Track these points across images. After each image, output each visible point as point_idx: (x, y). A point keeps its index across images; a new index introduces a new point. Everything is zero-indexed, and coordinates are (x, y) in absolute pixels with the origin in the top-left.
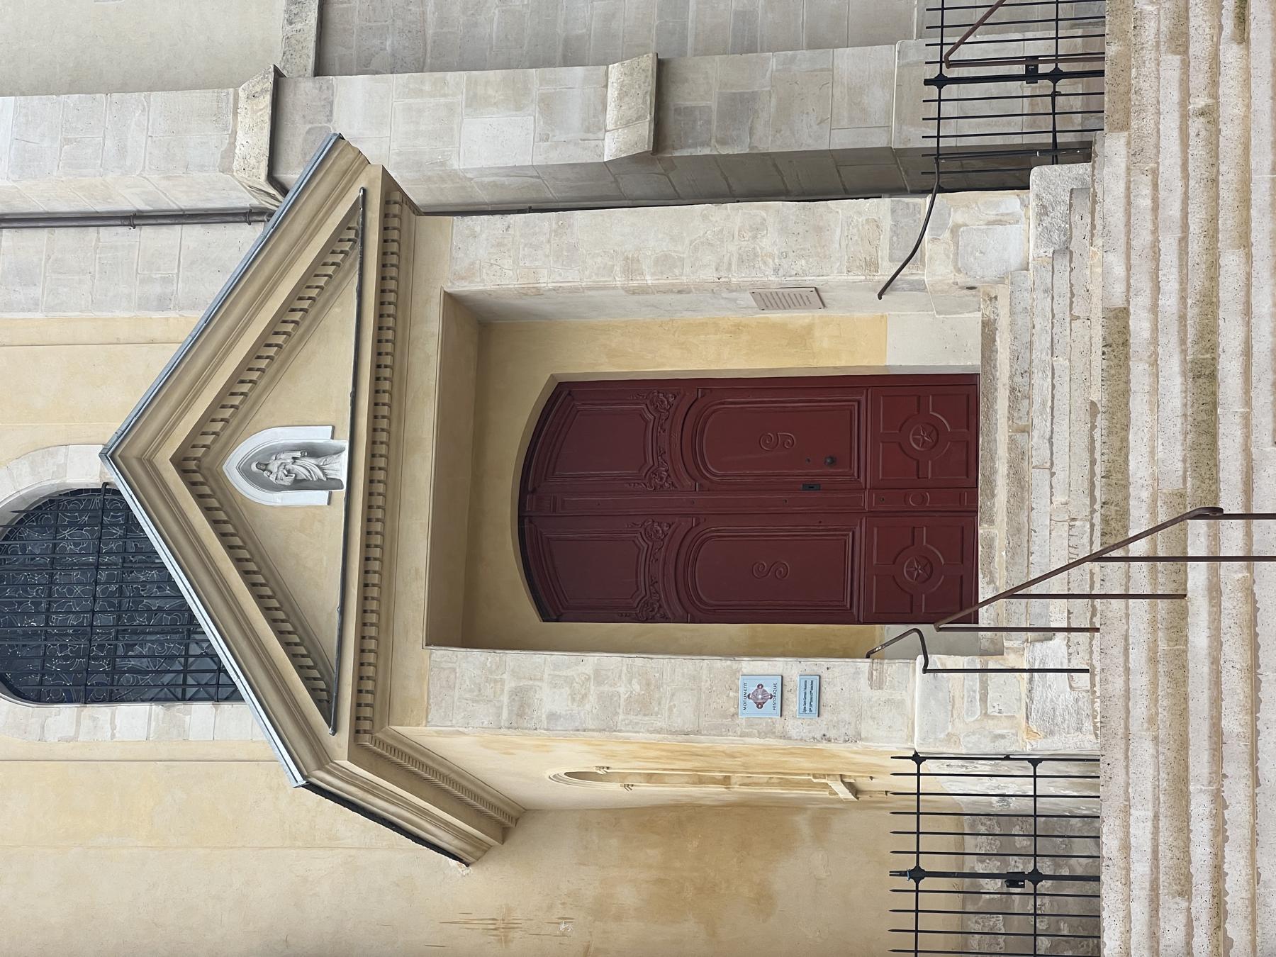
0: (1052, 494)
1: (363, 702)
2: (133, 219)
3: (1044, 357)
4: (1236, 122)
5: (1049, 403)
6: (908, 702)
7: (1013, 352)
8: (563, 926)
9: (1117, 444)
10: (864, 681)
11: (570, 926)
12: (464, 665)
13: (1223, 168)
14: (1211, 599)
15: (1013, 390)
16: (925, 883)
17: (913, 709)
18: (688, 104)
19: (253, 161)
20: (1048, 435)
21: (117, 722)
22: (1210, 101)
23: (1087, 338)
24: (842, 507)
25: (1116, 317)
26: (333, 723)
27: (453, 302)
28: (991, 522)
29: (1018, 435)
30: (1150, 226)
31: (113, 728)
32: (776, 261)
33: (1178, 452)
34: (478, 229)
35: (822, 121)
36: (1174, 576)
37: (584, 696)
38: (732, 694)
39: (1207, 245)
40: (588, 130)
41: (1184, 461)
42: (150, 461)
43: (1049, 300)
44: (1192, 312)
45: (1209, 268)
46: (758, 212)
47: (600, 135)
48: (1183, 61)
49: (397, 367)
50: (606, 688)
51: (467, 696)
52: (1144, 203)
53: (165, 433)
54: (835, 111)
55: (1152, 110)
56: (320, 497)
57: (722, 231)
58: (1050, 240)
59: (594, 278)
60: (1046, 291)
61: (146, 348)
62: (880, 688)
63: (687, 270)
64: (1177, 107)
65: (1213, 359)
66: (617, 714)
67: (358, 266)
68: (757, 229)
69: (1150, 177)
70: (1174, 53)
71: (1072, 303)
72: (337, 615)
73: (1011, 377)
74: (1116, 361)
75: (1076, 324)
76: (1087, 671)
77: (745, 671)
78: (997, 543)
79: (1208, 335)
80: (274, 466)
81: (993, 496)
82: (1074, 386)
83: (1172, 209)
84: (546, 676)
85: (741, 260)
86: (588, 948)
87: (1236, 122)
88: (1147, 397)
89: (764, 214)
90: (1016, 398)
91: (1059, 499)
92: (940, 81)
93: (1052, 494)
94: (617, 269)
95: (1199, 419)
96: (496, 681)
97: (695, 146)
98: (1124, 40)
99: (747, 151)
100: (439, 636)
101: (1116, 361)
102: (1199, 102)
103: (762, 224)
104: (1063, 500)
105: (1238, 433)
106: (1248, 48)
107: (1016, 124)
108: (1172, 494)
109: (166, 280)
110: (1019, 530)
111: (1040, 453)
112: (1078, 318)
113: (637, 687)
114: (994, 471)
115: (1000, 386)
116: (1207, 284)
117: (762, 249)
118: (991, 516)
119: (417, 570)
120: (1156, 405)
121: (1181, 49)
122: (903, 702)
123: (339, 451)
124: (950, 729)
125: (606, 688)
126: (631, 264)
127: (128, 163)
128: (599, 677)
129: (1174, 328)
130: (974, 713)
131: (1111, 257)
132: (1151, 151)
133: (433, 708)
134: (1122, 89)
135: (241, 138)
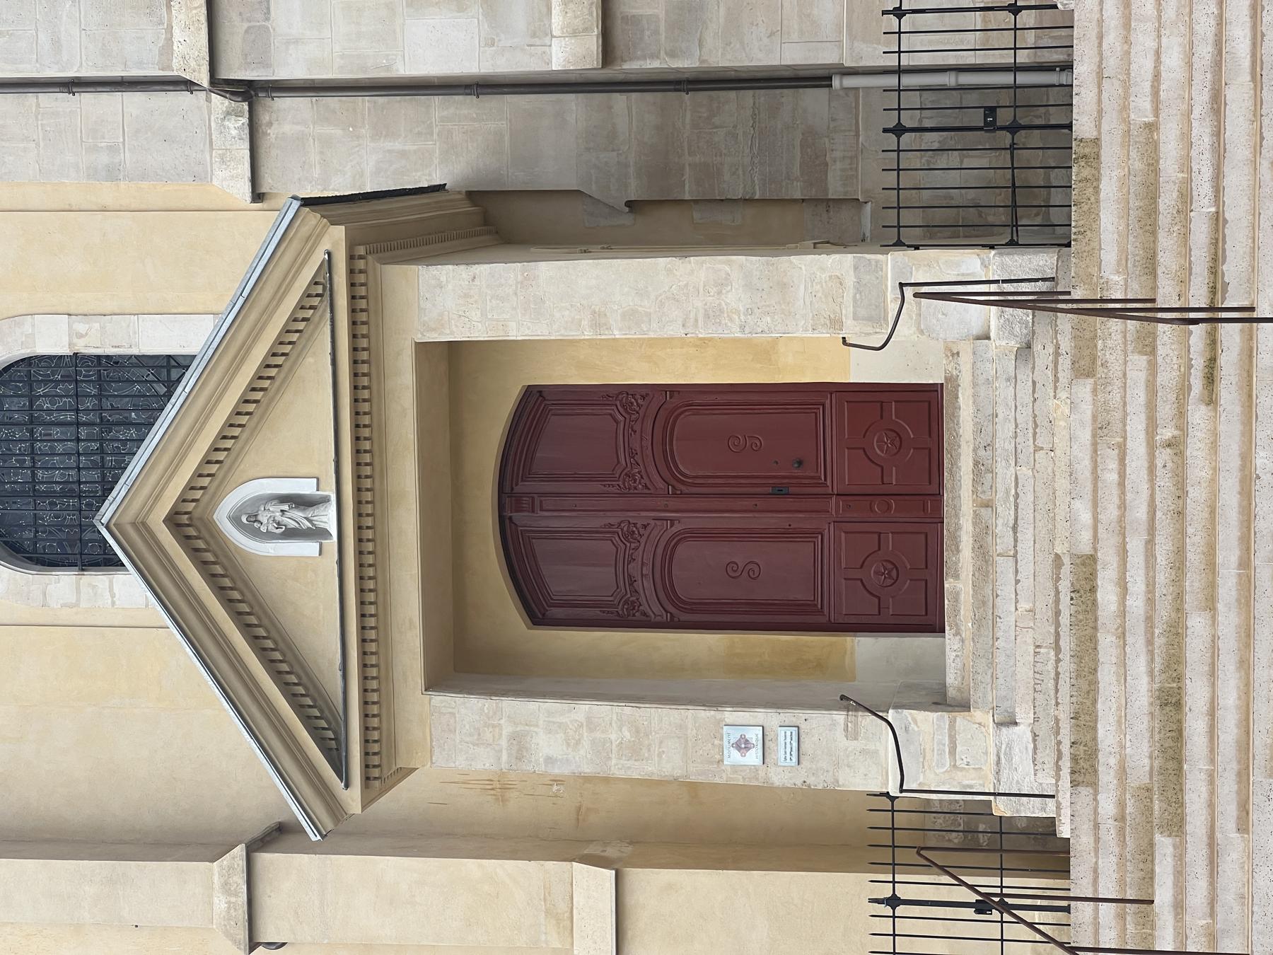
0: (1017, 602)
1: (371, 751)
2: (72, 85)
3: (1007, 446)
4: (1204, 485)
5: (1013, 492)
6: (882, 753)
7: (976, 424)
8: (555, 788)
9: (1085, 687)
10: (839, 733)
11: (562, 788)
12: (463, 711)
13: (1190, 530)
14: (1177, 914)
15: (976, 463)
16: (900, 910)
17: (886, 759)
18: (634, 12)
19: (193, 64)
20: (1011, 522)
21: (116, 590)
22: (1177, 433)
23: (1050, 470)
24: (809, 522)
25: (1083, 564)
26: (340, 766)
27: (423, 349)
28: (957, 577)
29: (983, 510)
30: (1116, 500)
31: (113, 596)
32: (742, 317)
33: (1145, 748)
34: (443, 279)
35: (772, 34)
36: (1141, 866)
37: (578, 742)
38: (716, 742)
39: (1173, 577)
40: (534, 35)
41: (1151, 757)
42: (144, 524)
43: (1011, 389)
44: (1159, 642)
45: (1175, 599)
46: (719, 266)
47: (547, 40)
48: (1149, 362)
49: (375, 426)
50: (598, 735)
51: (468, 739)
52: (1111, 477)
53: (156, 497)
54: (785, 22)
55: (1118, 383)
56: (308, 548)
57: (686, 285)
58: (1011, 333)
59: (563, 332)
60: (1008, 380)
61: (99, 215)
62: (856, 739)
63: (654, 325)
64: (1143, 409)
65: (1179, 688)
66: (610, 758)
67: (328, 315)
68: (722, 284)
69: (1116, 451)
70: (1141, 353)
71: (1035, 434)
72: (339, 674)
73: (975, 450)
74: (1084, 607)
75: (1040, 454)
76: (1053, 796)
77: (728, 721)
78: (962, 597)
79: (1177, 632)
80: (263, 518)
81: (958, 551)
82: (1038, 517)
83: (1140, 512)
84: (541, 722)
85: (707, 316)
86: (580, 808)
87: (1204, 485)
88: (1114, 669)
89: (727, 269)
90: (980, 472)
91: (1024, 605)
92: (899, 130)
93: (1017, 602)
94: (585, 323)
95: (1166, 745)
96: (494, 726)
97: (644, 58)
98: (1090, 284)
99: (697, 65)
100: (436, 681)
101: (1084, 607)
102: (1166, 433)
103: (726, 279)
104: (1028, 607)
105: (1204, 790)
106: (1215, 410)
107: (970, 40)
108: (1139, 788)
109: (112, 149)
110: (984, 603)
111: (1004, 540)
112: (1042, 449)
113: (627, 734)
114: (958, 527)
115: (963, 443)
116: (1173, 615)
117: (727, 304)
118: (956, 571)
119: (411, 620)
120: (1123, 676)
121: (1148, 349)
122: (876, 752)
123: (325, 500)
124: (921, 780)
125: (598, 735)
126: (598, 320)
127: (65, 59)
128: (591, 724)
129: (1141, 629)
130: (943, 765)
131: (1077, 504)
132: (1117, 426)
133: (437, 751)
134: (1088, 335)
135: (177, 34)
